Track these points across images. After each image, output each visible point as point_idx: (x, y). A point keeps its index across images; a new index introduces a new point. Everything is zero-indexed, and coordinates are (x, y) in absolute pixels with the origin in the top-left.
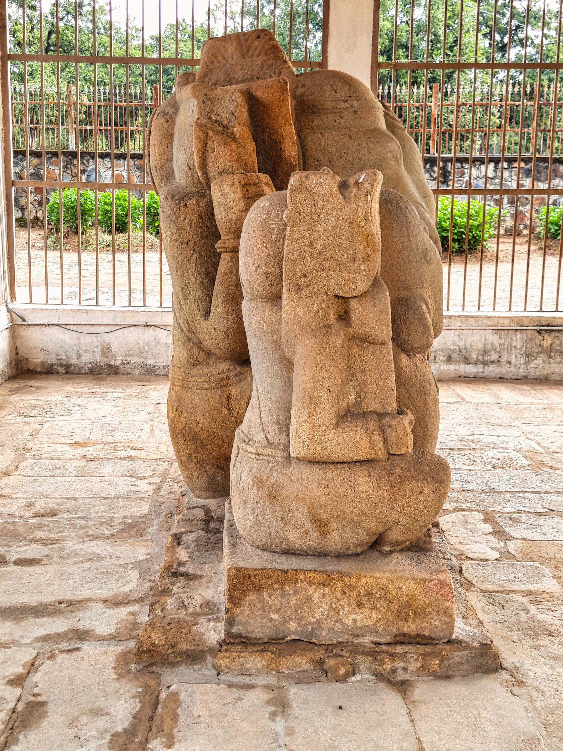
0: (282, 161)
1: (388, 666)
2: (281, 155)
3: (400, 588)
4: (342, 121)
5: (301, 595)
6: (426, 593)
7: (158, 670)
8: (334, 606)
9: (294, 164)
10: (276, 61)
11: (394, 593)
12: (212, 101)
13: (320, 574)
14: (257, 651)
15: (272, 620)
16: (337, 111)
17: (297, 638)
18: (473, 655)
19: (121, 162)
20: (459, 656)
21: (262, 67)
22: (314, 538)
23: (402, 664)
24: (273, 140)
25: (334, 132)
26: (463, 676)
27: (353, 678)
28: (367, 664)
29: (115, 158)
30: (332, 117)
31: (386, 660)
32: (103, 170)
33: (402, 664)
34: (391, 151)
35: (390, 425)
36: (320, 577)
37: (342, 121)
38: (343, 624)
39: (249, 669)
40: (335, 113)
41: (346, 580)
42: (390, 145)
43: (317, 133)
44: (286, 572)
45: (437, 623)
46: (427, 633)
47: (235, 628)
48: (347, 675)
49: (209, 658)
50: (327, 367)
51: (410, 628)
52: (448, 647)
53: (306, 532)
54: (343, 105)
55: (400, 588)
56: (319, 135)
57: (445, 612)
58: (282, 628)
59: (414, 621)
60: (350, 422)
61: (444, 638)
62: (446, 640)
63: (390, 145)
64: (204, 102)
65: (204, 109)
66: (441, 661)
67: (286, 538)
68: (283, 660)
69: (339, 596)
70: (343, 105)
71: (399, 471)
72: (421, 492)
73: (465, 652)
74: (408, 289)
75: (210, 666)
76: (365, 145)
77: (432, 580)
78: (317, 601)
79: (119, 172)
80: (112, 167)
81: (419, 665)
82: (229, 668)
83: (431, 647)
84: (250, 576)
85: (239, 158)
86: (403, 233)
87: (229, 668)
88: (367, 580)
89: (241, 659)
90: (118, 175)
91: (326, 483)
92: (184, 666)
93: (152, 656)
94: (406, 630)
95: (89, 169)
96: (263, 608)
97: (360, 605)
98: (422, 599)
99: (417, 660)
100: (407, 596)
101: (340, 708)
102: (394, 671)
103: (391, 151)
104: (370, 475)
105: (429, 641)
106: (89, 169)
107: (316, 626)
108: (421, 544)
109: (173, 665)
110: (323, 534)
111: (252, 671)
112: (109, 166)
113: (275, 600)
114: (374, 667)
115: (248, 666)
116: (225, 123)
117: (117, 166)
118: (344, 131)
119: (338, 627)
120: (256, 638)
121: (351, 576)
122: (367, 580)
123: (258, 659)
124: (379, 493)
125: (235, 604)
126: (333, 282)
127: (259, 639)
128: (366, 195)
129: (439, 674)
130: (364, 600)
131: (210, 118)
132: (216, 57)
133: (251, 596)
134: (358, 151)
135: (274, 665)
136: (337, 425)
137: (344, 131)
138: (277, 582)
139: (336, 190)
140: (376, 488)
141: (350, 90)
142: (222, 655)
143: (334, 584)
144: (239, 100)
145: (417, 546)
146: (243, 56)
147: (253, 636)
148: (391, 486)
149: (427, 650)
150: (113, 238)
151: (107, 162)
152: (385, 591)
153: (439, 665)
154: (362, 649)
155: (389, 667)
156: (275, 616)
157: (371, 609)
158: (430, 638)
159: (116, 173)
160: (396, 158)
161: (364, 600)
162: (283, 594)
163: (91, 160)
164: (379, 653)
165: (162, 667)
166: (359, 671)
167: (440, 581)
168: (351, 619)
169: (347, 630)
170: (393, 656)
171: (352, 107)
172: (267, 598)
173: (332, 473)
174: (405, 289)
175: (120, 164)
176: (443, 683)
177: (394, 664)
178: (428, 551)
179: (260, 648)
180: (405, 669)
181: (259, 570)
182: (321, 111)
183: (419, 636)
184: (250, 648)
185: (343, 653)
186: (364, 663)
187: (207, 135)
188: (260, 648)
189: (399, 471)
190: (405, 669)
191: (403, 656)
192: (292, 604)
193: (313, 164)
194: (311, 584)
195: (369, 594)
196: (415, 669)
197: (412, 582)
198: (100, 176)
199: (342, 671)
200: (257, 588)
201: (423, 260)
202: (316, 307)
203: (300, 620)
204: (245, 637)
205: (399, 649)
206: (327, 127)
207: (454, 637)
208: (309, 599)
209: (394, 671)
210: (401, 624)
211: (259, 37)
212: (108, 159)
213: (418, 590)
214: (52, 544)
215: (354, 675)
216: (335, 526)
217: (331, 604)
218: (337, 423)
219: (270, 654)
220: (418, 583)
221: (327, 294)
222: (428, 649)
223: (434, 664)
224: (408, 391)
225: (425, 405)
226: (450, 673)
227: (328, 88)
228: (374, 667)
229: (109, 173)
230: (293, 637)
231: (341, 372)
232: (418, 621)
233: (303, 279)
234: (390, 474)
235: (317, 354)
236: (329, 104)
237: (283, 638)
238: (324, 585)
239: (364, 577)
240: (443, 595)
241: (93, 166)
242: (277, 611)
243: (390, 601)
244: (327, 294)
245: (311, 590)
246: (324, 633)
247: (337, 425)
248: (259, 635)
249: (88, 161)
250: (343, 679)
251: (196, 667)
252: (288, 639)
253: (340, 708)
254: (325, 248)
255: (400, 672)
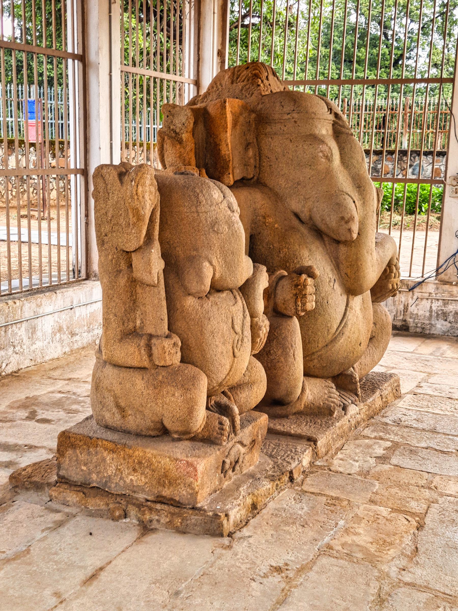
0: (220, 158)
1: (147, 517)
2: (219, 153)
3: (160, 462)
4: (285, 129)
5: (99, 456)
6: (177, 469)
7: (19, 491)
8: (119, 468)
9: (228, 160)
10: (253, 85)
11: (156, 465)
12: (173, 116)
13: (111, 443)
14: (76, 491)
15: (82, 470)
16: (282, 121)
17: (97, 486)
18: (206, 521)
19: (441, 158)
20: (194, 518)
21: (242, 90)
22: (118, 419)
23: (157, 517)
24: (215, 143)
25: (280, 137)
26: (196, 535)
27: (124, 520)
28: (134, 512)
29: (424, 154)
30: (278, 126)
31: (146, 512)
32: (425, 165)
33: (157, 517)
34: (321, 151)
35: (155, 344)
36: (110, 445)
37: (285, 129)
38: (125, 482)
39: (68, 501)
40: (281, 123)
41: (127, 450)
42: (321, 146)
43: (269, 137)
44: (91, 438)
45: (184, 492)
46: (177, 498)
47: (61, 471)
48: (120, 517)
49: (46, 489)
50: (114, 299)
51: (166, 492)
52: (190, 512)
53: (114, 413)
54: (286, 117)
55: (160, 462)
56: (270, 139)
57: (189, 485)
58: (88, 477)
59: (169, 488)
60: (131, 339)
61: (189, 505)
62: (191, 506)
63: (321, 146)
64: (168, 117)
65: (167, 122)
66: (182, 520)
67: (104, 416)
68: (89, 500)
69: (122, 461)
70: (286, 117)
71: (160, 378)
72: (174, 395)
73: (201, 518)
74: (196, 250)
75: (47, 495)
76: (301, 146)
77: (182, 460)
78: (108, 462)
79: (438, 167)
80: (433, 162)
81: (168, 520)
82: (56, 498)
83: (179, 509)
84: (69, 437)
85: (180, 155)
86: (192, 210)
87: (56, 498)
88: (139, 453)
89: (64, 494)
90: (437, 169)
91: (120, 380)
92: (32, 491)
93: (16, 481)
94: (164, 494)
95: (415, 164)
96: (77, 460)
97: (135, 470)
98: (174, 473)
99: (167, 516)
100: (165, 469)
101: (91, 534)
102: (151, 521)
103: (321, 151)
104: (143, 379)
105: (179, 505)
106: (415, 164)
107: (108, 480)
108: (212, 439)
109: (27, 489)
110: (123, 417)
111: (70, 503)
112: (431, 161)
113: (83, 457)
114: (139, 516)
115: (68, 499)
116: (178, 130)
117: (437, 162)
118: (287, 136)
119: (121, 483)
120: (73, 481)
121: (130, 448)
122: (139, 453)
123: (75, 496)
124: (148, 392)
125: (61, 455)
126: (120, 240)
127: (75, 482)
128: (132, 181)
129: (180, 530)
130: (137, 467)
131: (170, 127)
132: (216, 84)
133: (70, 452)
134: (296, 151)
135: (83, 502)
136: (121, 340)
137: (287, 136)
138: (85, 444)
139: (117, 178)
140: (146, 388)
141: (294, 105)
142: (54, 488)
143: (119, 452)
144: (189, 114)
145: (208, 440)
146: (232, 83)
147: (72, 479)
148: (155, 388)
149: (176, 511)
150: (402, 218)
151: (430, 158)
152: (151, 464)
153: (181, 523)
154: (134, 501)
155: (148, 517)
156: (84, 468)
157: (141, 474)
158: (179, 502)
159: (435, 167)
160: (327, 156)
161: (137, 467)
162: (89, 453)
163: (417, 157)
164: (143, 506)
165: (21, 489)
166: (130, 516)
167: (187, 462)
168: (129, 479)
169: (126, 487)
170: (151, 509)
171: (293, 118)
172: (79, 454)
173: (125, 374)
174: (194, 250)
175: (439, 160)
176: (177, 535)
177: (152, 516)
178: (217, 444)
179: (78, 489)
180: (158, 521)
181: (76, 434)
182: (272, 121)
183: (172, 499)
184: (73, 488)
185: (122, 502)
186: (133, 511)
187: (164, 139)
188: (78, 489)
189: (160, 378)
190: (158, 521)
191: (158, 511)
192: (93, 461)
193: (265, 161)
194: (106, 449)
195: (140, 463)
196: (164, 522)
197: (168, 459)
198: (423, 169)
199: (117, 514)
200: (73, 446)
201: (211, 230)
202: (110, 257)
203: (99, 473)
204: (67, 479)
205: (158, 506)
206: (275, 134)
207: (199, 505)
208: (104, 460)
209: (151, 521)
210: (160, 488)
211: (248, 68)
212: (430, 156)
213: (171, 466)
214: (72, 413)
215: (125, 518)
216: (130, 412)
217: (117, 466)
218: (122, 338)
219: (82, 494)
220: (172, 461)
221: (116, 248)
222: (177, 510)
223: (178, 521)
224: (187, 323)
225: (201, 335)
226: (188, 530)
227: (278, 104)
228: (139, 516)
229: (430, 167)
230: (95, 485)
231: (124, 303)
232: (171, 489)
233: (105, 237)
234: (155, 379)
235: (109, 289)
236: (277, 116)
237: (89, 484)
238: (113, 452)
239: (138, 450)
240: (188, 473)
241: (418, 162)
242: (85, 465)
243: (153, 471)
244: (116, 248)
245: (105, 454)
246: (113, 485)
247: (121, 340)
248: (75, 479)
249: (414, 158)
250: (114, 519)
251: (40, 494)
252: (92, 485)
253: (91, 534)
254: (113, 217)
255: (155, 522)
